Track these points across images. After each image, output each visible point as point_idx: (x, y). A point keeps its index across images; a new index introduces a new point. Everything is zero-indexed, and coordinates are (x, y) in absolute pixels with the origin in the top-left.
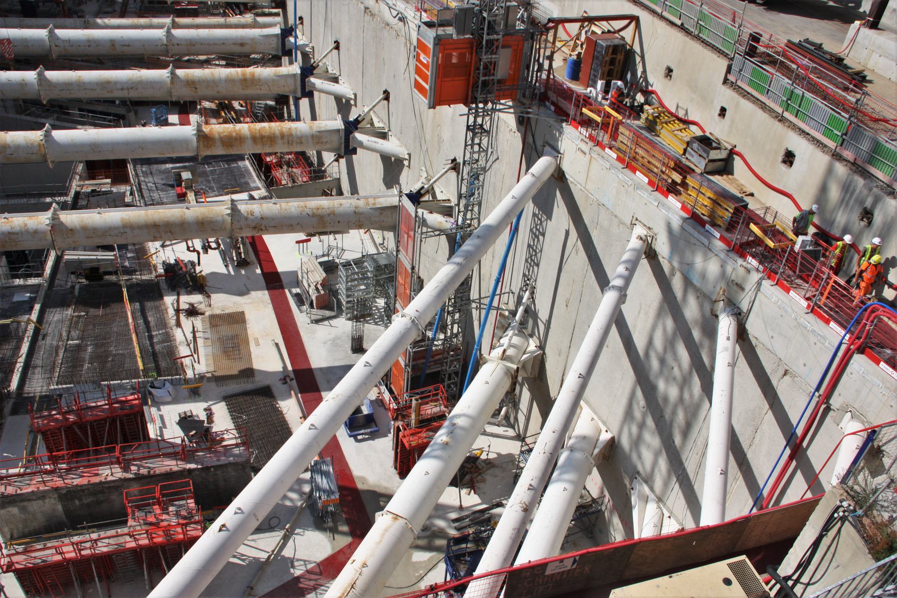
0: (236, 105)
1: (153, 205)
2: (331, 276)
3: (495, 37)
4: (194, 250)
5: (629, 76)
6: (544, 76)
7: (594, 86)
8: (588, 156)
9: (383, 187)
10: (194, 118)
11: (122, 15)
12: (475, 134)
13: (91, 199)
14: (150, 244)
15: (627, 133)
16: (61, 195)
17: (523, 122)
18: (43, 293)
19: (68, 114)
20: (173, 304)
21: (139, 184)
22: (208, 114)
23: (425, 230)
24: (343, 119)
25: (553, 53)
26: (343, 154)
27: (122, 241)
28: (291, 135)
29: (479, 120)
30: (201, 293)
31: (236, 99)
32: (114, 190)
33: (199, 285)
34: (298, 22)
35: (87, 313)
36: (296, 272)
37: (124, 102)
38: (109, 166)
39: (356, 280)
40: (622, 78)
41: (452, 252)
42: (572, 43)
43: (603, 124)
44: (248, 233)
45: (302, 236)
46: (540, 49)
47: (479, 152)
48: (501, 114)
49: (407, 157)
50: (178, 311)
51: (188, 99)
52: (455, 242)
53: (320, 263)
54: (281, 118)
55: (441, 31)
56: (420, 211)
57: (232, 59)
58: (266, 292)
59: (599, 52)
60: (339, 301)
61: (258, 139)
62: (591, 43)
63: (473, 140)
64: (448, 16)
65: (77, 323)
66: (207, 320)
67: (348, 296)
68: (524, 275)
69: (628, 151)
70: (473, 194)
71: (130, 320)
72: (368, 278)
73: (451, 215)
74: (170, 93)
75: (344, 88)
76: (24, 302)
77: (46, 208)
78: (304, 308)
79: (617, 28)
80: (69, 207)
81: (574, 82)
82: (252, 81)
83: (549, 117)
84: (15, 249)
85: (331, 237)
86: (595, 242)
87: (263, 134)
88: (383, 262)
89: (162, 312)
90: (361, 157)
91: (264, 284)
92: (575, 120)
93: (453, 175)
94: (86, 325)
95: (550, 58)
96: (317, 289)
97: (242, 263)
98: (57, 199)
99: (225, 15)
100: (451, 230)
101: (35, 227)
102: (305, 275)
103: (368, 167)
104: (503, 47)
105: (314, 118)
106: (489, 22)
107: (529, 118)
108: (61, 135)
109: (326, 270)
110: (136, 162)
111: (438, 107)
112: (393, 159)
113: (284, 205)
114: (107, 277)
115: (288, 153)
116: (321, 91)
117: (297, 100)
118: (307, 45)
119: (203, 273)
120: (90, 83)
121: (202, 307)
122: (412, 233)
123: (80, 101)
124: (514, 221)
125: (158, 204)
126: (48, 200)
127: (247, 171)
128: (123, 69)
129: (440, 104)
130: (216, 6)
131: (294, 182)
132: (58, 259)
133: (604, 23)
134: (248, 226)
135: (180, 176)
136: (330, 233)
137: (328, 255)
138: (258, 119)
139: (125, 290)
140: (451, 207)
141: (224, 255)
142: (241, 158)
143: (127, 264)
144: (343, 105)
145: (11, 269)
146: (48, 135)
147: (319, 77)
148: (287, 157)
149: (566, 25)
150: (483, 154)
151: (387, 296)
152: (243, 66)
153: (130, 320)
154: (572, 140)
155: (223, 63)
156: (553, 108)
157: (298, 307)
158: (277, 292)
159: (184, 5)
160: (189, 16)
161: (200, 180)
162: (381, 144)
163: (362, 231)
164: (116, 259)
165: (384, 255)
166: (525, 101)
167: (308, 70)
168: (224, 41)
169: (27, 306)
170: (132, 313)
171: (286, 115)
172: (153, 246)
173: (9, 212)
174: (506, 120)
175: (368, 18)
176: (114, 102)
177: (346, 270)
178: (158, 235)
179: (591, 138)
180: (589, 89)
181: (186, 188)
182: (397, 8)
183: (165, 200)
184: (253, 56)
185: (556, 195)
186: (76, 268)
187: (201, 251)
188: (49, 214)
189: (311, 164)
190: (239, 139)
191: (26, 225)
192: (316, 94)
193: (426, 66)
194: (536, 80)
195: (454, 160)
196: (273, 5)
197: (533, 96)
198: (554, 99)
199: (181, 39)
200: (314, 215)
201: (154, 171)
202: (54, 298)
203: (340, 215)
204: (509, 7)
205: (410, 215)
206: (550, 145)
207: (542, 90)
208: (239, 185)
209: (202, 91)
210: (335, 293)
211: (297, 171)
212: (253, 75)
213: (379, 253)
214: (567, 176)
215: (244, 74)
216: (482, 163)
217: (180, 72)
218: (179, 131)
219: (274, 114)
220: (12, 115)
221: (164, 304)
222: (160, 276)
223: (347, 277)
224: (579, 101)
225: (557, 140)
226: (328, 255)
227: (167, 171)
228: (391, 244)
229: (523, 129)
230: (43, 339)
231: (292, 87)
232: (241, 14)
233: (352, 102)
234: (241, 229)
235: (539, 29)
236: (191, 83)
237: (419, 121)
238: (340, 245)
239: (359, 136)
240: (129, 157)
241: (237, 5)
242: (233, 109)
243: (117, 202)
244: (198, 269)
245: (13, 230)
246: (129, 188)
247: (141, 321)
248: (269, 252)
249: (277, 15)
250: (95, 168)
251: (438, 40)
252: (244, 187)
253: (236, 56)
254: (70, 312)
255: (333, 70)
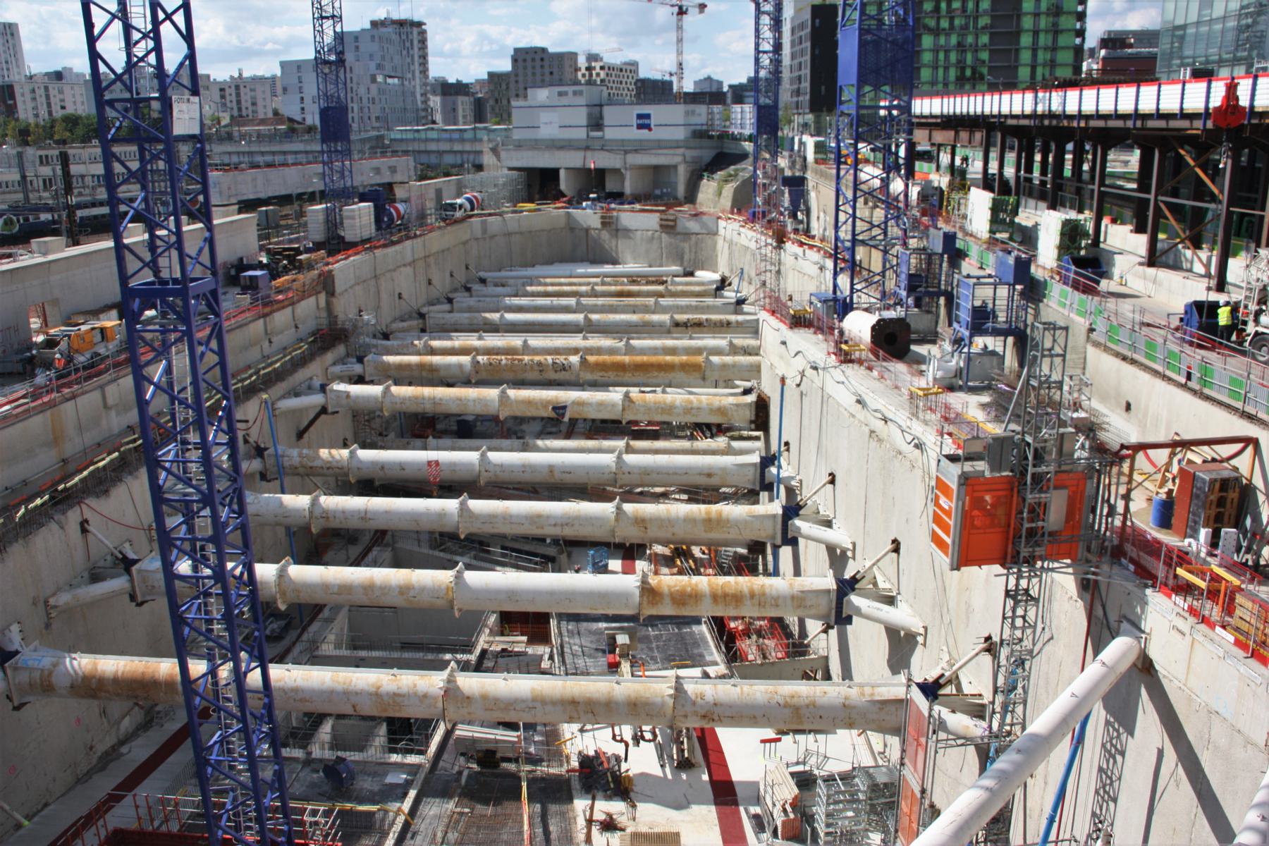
0: (696, 551)
1: (576, 674)
2: (806, 794)
3: (1044, 469)
4: (622, 741)
5: (1248, 522)
6: (1118, 522)
7: (1194, 535)
8: (1188, 639)
9: (887, 672)
10: (641, 565)
11: (568, 436)
12: (1017, 603)
13: (500, 660)
14: (566, 725)
15: (1249, 605)
16: (464, 652)
17: (1087, 587)
18: (423, 776)
19: (488, 552)
20: (584, 812)
21: (562, 646)
22: (658, 560)
23: (942, 735)
24: (835, 576)
25: (1129, 491)
26: (832, 623)
27: (530, 720)
28: (764, 594)
29: (1024, 583)
30: (624, 800)
31: (696, 544)
32: (530, 650)
33: (621, 788)
34: (783, 448)
35: (472, 809)
36: (756, 784)
37: (556, 541)
38: (530, 622)
39: (841, 802)
40: (1238, 523)
41: (983, 769)
42: (1159, 476)
43: (1209, 592)
44: (694, 723)
45: (770, 733)
46: (1110, 485)
47: (1023, 629)
48: (1054, 575)
49: (922, 631)
50: (590, 822)
51: (636, 541)
52: (987, 757)
53: (793, 774)
54: (753, 571)
55: (968, 466)
56: (937, 708)
57: (697, 493)
58: (713, 808)
59: (1199, 489)
60: (814, 831)
61: (716, 597)
62: (1187, 476)
63: (1014, 611)
64: (977, 447)
65: (458, 822)
66: (628, 839)
67: (828, 825)
68: (1094, 814)
69: (1253, 631)
70: (1015, 688)
71: (526, 827)
72: (858, 801)
73: (982, 717)
74: (613, 532)
75: (840, 536)
76: (398, 785)
77: (442, 666)
78: (764, 836)
79: (1225, 455)
80: (472, 668)
81: (1165, 531)
82: (720, 522)
83: (1127, 580)
84: (397, 715)
85: (811, 737)
86: (1206, 770)
87: (727, 590)
88: (882, 779)
89: (568, 821)
90: (856, 629)
91: (712, 797)
92: (1166, 585)
93: (987, 659)
94: (468, 827)
95: (1127, 497)
96: (785, 810)
97: (684, 764)
98: (459, 656)
99: (692, 438)
100: (982, 738)
101: (425, 690)
102: (769, 789)
103: (867, 643)
104: (1056, 488)
105: (797, 572)
106: (1036, 450)
107: (1096, 582)
108: (475, 578)
109: (799, 785)
110: (561, 617)
111: (963, 569)
112: (902, 633)
113: (746, 688)
114: (504, 765)
115: (760, 619)
116: (808, 538)
117: (776, 548)
118: (793, 478)
119: (630, 773)
120: (518, 516)
121: (622, 820)
122: (923, 740)
123: (504, 537)
124: (1077, 728)
125: (582, 674)
126: (448, 656)
127: (703, 638)
128: (560, 500)
129: (966, 565)
130: (682, 427)
131: (765, 657)
132: (448, 734)
133: (1206, 448)
134: (696, 714)
135: (614, 639)
136: (810, 732)
137: (804, 763)
138: (723, 571)
139: (524, 785)
140: (983, 706)
141: (661, 751)
142: (697, 621)
143: (532, 750)
144: (837, 557)
145: (391, 741)
146: (459, 577)
147: (806, 519)
148: (758, 623)
149: (1150, 452)
150: (1029, 631)
151: (885, 831)
152: (710, 502)
153: (526, 827)
154: (1162, 614)
155: (685, 497)
156: (1132, 567)
157: (756, 834)
158: (728, 809)
159: (643, 426)
160: (647, 439)
161: (640, 646)
162: (886, 612)
163: (855, 732)
164: (519, 742)
165: (884, 770)
166: (1090, 556)
167: (792, 510)
168: (686, 471)
169: (400, 791)
170: (530, 818)
171: (761, 567)
172: (568, 729)
173: (400, 668)
174: (1061, 585)
175: (873, 444)
176: (544, 540)
177: (829, 787)
178: (575, 715)
179: (1192, 611)
180: (1187, 541)
181: (621, 656)
182: (913, 432)
183: (592, 670)
184: (723, 490)
185: (1140, 695)
186: (469, 749)
187: (631, 742)
188: (444, 675)
189: (789, 635)
190: (694, 597)
191: (415, 686)
192: (801, 541)
193: (948, 513)
194: (1106, 529)
195: (988, 638)
196: (753, 426)
197: (1102, 550)
198: (1134, 555)
199: (634, 467)
200: (786, 705)
201: (582, 630)
202: (435, 785)
203: (823, 707)
204: (1063, 435)
205: (920, 713)
206: (1129, 621)
207: (1116, 542)
208: (691, 657)
209: (653, 532)
210: (809, 819)
211: (770, 643)
212: (720, 514)
213: (877, 766)
214: (1157, 667)
215: (708, 513)
216: (1027, 643)
217: (627, 507)
218: (619, 581)
219: (745, 566)
220: (425, 550)
221: (573, 811)
222: (573, 770)
223: (829, 797)
224: (1171, 558)
225: (1140, 618)
226: (804, 763)
227: (599, 632)
228: (895, 754)
229: (1088, 596)
230: (412, 838)
231: (770, 532)
232: (712, 437)
233: (849, 554)
234: (686, 716)
235: (1112, 457)
236: (641, 522)
237: (940, 583)
238: (822, 750)
239: (855, 599)
240: (554, 610)
241: (709, 426)
242: (692, 556)
243: (530, 666)
244: (624, 766)
245: (400, 691)
246: (548, 650)
247: (539, 831)
248: (722, 753)
249: (757, 438)
250: (511, 621)
251: (965, 479)
252: (695, 660)
253: (702, 490)
254: (450, 805)
255: (826, 511)
